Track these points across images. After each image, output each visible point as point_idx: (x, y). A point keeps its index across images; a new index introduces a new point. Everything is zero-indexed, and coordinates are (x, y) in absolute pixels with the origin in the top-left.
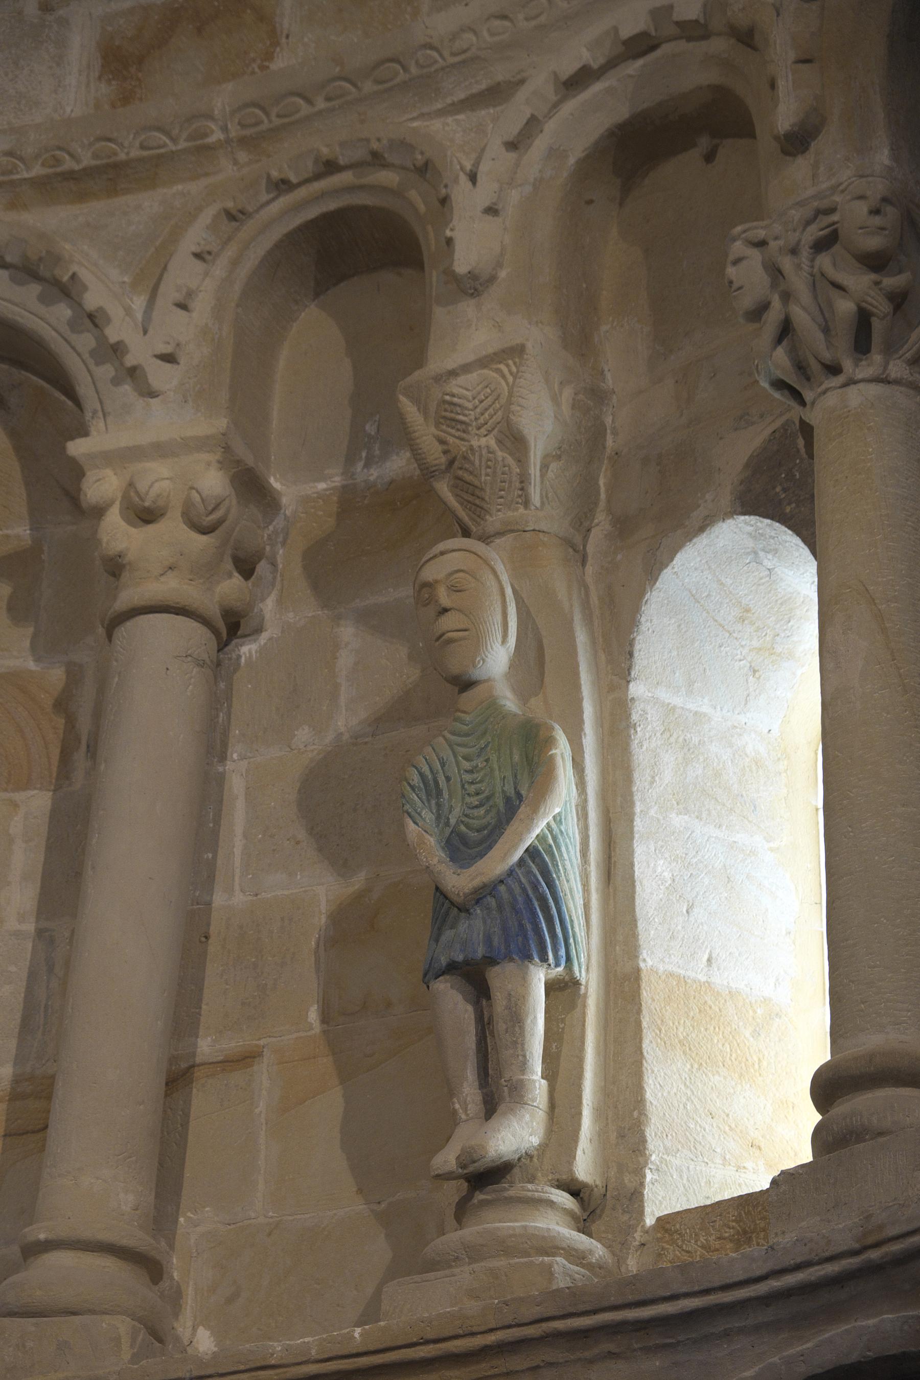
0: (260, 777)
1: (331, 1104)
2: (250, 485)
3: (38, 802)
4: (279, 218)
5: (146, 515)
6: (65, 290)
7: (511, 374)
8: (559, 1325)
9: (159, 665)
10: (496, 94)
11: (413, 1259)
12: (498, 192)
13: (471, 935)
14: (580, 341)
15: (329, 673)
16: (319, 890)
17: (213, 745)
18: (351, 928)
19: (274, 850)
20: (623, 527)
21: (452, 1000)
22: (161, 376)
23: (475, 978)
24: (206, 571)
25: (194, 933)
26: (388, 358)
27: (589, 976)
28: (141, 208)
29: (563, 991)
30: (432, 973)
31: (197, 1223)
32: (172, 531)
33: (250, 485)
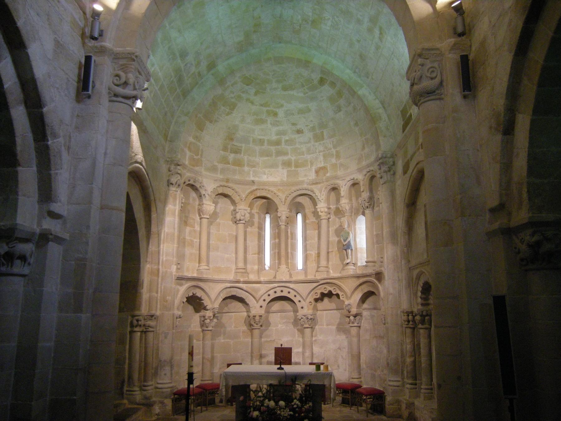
1: (338, 255)
2: (329, 208)
3: (317, 231)
4: (329, 188)
7: (344, 203)
8: (329, 281)
9: (324, 223)
11: (343, 269)
12: (344, 190)
13: (345, 247)
14: (351, 200)
15: (335, 222)
17: (328, 227)
19: (334, 189)
20: (355, 214)
21: (344, 251)
22: (322, 201)
23: (346, 250)
24: (326, 216)
25: (328, 242)
26: (338, 200)
27: (353, 249)
28: (319, 186)
29: (352, 250)
31: (330, 263)
32: (324, 213)
33: (329, 208)
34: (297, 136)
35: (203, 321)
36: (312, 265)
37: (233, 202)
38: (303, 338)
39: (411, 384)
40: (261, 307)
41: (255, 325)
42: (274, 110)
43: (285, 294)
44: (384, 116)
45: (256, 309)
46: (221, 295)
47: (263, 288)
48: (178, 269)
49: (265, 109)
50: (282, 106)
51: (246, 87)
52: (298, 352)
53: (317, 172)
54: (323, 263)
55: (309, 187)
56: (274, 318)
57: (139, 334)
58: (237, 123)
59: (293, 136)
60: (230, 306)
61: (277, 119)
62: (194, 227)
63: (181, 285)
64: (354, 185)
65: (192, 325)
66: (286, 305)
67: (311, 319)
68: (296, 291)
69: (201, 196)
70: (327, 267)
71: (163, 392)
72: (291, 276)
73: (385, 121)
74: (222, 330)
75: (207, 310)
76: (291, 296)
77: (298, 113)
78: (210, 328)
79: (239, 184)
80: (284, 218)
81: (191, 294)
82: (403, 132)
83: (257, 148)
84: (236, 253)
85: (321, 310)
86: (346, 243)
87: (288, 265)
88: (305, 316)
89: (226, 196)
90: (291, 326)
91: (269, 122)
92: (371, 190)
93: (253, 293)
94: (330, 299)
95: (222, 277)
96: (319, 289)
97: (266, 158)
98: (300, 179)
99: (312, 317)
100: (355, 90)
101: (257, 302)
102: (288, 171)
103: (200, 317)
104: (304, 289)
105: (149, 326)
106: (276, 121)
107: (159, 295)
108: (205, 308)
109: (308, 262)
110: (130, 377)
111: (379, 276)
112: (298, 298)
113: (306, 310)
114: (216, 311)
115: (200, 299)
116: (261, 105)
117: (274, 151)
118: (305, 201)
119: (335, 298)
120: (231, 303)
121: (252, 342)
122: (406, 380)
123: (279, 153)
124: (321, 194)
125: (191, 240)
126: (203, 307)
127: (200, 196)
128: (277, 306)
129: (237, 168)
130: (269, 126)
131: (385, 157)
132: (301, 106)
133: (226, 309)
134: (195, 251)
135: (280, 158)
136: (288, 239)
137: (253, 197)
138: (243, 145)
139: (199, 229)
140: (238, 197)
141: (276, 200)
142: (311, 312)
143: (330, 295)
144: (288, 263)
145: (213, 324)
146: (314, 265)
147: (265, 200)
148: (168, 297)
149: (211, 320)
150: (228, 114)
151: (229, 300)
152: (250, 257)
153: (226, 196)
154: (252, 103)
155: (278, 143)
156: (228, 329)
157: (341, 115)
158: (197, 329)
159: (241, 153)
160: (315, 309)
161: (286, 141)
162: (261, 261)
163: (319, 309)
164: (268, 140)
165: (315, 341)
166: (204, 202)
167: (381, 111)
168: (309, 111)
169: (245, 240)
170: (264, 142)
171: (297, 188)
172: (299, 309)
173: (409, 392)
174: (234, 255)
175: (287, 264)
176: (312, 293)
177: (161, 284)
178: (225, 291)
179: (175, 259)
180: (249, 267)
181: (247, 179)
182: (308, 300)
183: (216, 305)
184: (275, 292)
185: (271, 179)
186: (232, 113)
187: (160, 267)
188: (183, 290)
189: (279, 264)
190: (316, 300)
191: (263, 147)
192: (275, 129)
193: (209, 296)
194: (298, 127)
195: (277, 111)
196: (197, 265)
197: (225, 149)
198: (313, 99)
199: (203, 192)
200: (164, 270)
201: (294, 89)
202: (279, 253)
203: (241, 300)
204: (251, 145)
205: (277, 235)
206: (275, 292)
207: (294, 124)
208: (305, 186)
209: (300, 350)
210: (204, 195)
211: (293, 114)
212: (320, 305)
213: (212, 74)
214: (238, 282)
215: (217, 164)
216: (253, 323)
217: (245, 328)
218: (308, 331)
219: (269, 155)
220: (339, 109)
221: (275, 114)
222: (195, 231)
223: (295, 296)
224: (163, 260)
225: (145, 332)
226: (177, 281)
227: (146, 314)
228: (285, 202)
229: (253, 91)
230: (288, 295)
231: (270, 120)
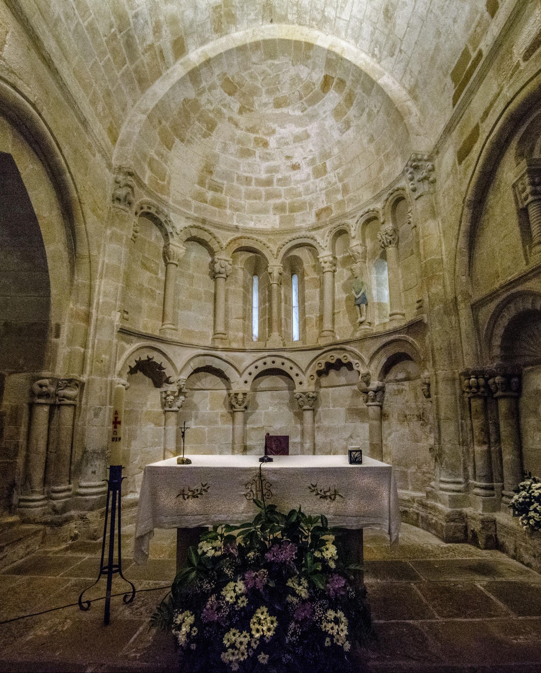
0: (338, 285)
1: (347, 316)
2: (335, 258)
3: (318, 290)
4: (334, 231)
5: (326, 263)
6: (316, 240)
9: (328, 277)
10: (354, 217)
13: (358, 301)
15: (343, 273)
16: (344, 296)
18: (348, 299)
20: (370, 259)
21: (357, 308)
24: (331, 267)
30: (355, 305)
31: (336, 327)
32: (328, 264)
33: (335, 258)
34: (292, 173)
35: (165, 398)
36: (313, 331)
37: (212, 252)
38: (302, 424)
39: (485, 488)
40: (246, 382)
41: (237, 406)
42: (264, 137)
43: (278, 365)
44: (415, 110)
45: (239, 384)
46: (192, 364)
47: (248, 359)
48: (123, 319)
49: (252, 136)
50: (274, 132)
51: (228, 98)
52: (295, 443)
53: (318, 215)
54: (327, 325)
55: (308, 234)
56: (263, 398)
57: (46, 409)
58: (217, 151)
59: (287, 174)
60: (203, 380)
61: (268, 151)
62: (157, 274)
63: (129, 342)
64: (368, 221)
65: (148, 403)
66: (280, 382)
67: (313, 397)
68: (292, 362)
69: (167, 235)
70: (333, 331)
71: (87, 501)
72: (284, 345)
73: (416, 115)
74: (193, 413)
75: (171, 383)
76: (286, 368)
77: (294, 142)
78: (175, 408)
79: (219, 228)
80: (276, 274)
81: (144, 358)
82: (454, 105)
83: (243, 188)
84: (215, 316)
85: (325, 387)
86: (359, 295)
87: (281, 333)
88: (304, 393)
89: (202, 243)
90: (286, 409)
91: (257, 154)
92: (394, 220)
93: (235, 364)
94: (337, 372)
95: (195, 342)
96: (323, 359)
97: (255, 201)
98: (297, 225)
99: (314, 395)
100: (374, 79)
101: (241, 375)
102: (281, 217)
103: (161, 393)
104: (303, 359)
105: (64, 397)
106: (267, 153)
107: (90, 351)
108: (167, 381)
109: (307, 328)
110: (28, 478)
111: (416, 327)
112: (296, 370)
113: (305, 385)
114: (182, 383)
115: (160, 367)
116: (248, 130)
117: (264, 193)
118: (303, 254)
119: (344, 369)
120: (206, 377)
121: (233, 429)
122: (471, 481)
123: (270, 196)
124: (323, 240)
125: (152, 291)
126: (164, 379)
127: (166, 236)
128: (266, 382)
129: (217, 209)
130: (258, 159)
131: (420, 160)
132: (298, 130)
133: (198, 385)
134: (157, 305)
135: (272, 202)
136: (281, 302)
137: (236, 246)
138: (225, 182)
139: (164, 278)
140: (217, 245)
141: (265, 252)
142: (312, 388)
143: (338, 365)
144: (281, 331)
145: (179, 403)
146: (316, 331)
147: (251, 254)
148: (103, 356)
149: (175, 397)
150: (205, 136)
151: (202, 374)
152: (233, 322)
153: (202, 243)
154: (236, 125)
155: (268, 182)
156: (202, 411)
157: (351, 133)
158: (156, 410)
159: (222, 192)
160: (318, 384)
161: (279, 180)
162: (247, 329)
163: (323, 385)
164: (256, 179)
165: (318, 428)
166: (171, 241)
167: (410, 103)
168: (308, 136)
169: (226, 300)
170: (251, 181)
171: (294, 235)
172: (297, 383)
173: (484, 502)
174: (212, 318)
175: (280, 331)
176: (314, 363)
177: (95, 336)
178: (197, 360)
179: (118, 303)
180: (231, 333)
181: (230, 223)
182: (309, 373)
183: (184, 376)
184: (265, 363)
185: (260, 226)
186: (210, 135)
187: (94, 311)
188: (131, 349)
189: (270, 331)
190: (320, 373)
191: (250, 187)
192: (265, 165)
193: (173, 365)
194: (294, 161)
195: (268, 139)
196: (161, 323)
197: (202, 183)
198: (313, 117)
199: (170, 229)
200: (100, 316)
201: (289, 105)
202: (270, 319)
203: (219, 373)
204: (235, 183)
205: (267, 299)
206: (256, 367)
207: (288, 157)
208: (303, 233)
209: (298, 439)
210: (171, 233)
211: (287, 144)
212: (324, 381)
213: (181, 64)
214: (216, 349)
215: (190, 199)
216: (234, 403)
217: (224, 411)
218: (308, 415)
219: (256, 196)
220: (348, 125)
221: (266, 144)
222: (158, 280)
223: (291, 368)
224: (98, 303)
225: (59, 406)
226: (121, 335)
227: (62, 378)
228: (277, 255)
229: (236, 106)
230: (282, 368)
231: (259, 151)
